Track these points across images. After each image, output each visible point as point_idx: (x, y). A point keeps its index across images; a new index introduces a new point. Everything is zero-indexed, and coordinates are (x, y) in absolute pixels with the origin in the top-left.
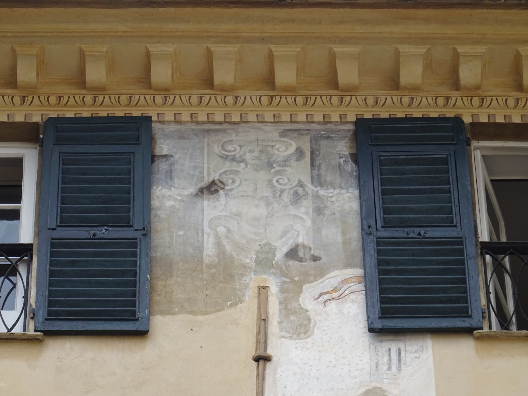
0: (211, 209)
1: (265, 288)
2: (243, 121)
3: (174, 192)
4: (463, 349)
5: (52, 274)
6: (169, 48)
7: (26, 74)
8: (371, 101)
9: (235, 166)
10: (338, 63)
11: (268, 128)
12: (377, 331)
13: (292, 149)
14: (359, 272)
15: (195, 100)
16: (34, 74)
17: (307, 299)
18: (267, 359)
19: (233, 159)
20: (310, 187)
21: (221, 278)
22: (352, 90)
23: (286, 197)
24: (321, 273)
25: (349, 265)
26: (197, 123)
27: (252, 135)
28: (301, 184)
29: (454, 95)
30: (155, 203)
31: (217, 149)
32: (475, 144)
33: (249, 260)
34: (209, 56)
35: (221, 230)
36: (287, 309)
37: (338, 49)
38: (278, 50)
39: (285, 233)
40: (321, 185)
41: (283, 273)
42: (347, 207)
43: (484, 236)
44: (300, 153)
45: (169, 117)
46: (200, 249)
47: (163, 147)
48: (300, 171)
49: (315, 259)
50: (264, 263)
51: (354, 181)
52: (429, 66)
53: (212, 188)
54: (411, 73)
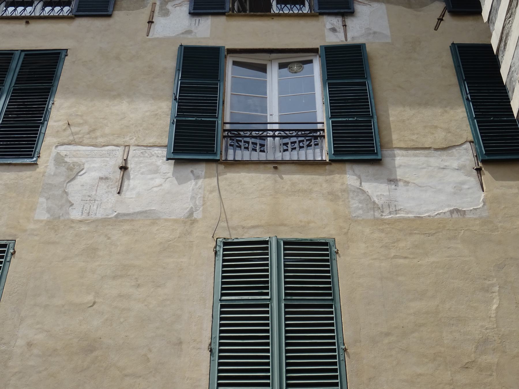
1: (155, 3)
4: (221, 20)
18: (152, 22)
36: (161, 9)
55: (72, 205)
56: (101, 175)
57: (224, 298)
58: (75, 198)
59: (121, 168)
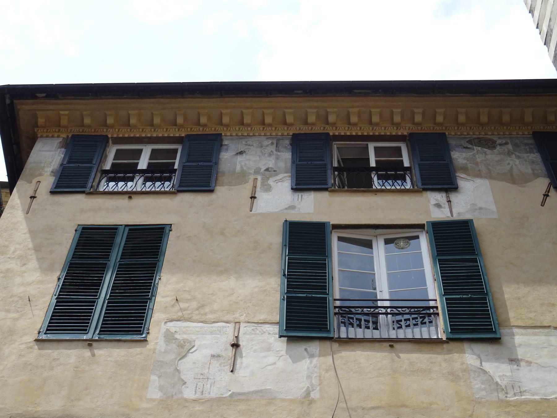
0: (239, 158)
2: (254, 135)
3: (228, 154)
5: (182, 175)
6: (228, 111)
7: (180, 120)
8: (298, 128)
9: (250, 147)
10: (287, 116)
11: (263, 137)
12: (295, 189)
13: (271, 142)
14: (290, 174)
15: (237, 129)
16: (182, 121)
17: (271, 182)
18: (255, 198)
19: (249, 145)
20: (275, 152)
21: (242, 177)
22: (291, 125)
23: (266, 155)
24: (277, 175)
25: (286, 172)
26: (238, 136)
27: (257, 139)
28: (272, 151)
29: (327, 126)
30: (221, 157)
31: (244, 143)
32: (334, 143)
33: (252, 171)
34: (242, 114)
35: (243, 164)
36: (263, 184)
37: (286, 110)
38: (266, 111)
39: (265, 164)
40: (279, 152)
41: (262, 174)
42: (287, 157)
43: (335, 164)
44: (272, 144)
45: (228, 134)
46: (235, 169)
47: (225, 142)
48: (273, 148)
49: (275, 171)
50: (257, 171)
51: (291, 151)
52: (318, 117)
53: (241, 153)
54: (312, 119)
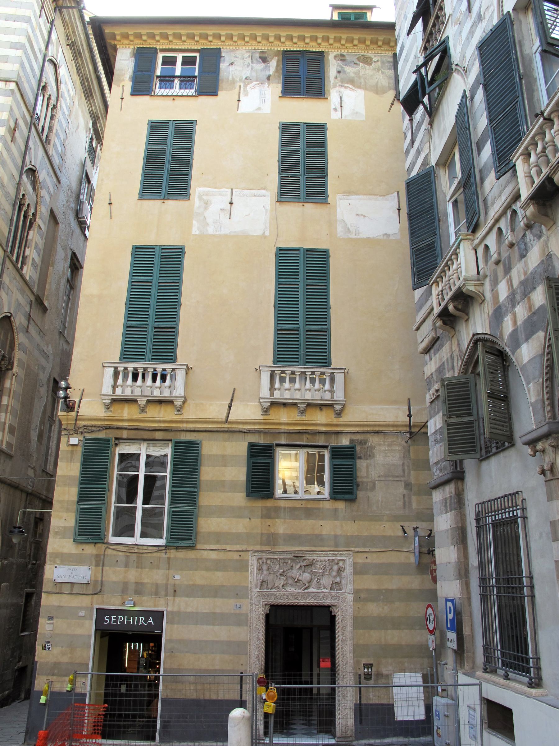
36: (244, 90)
55: (208, 224)
56: (221, 208)
57: (280, 280)
58: (210, 220)
59: (230, 203)
